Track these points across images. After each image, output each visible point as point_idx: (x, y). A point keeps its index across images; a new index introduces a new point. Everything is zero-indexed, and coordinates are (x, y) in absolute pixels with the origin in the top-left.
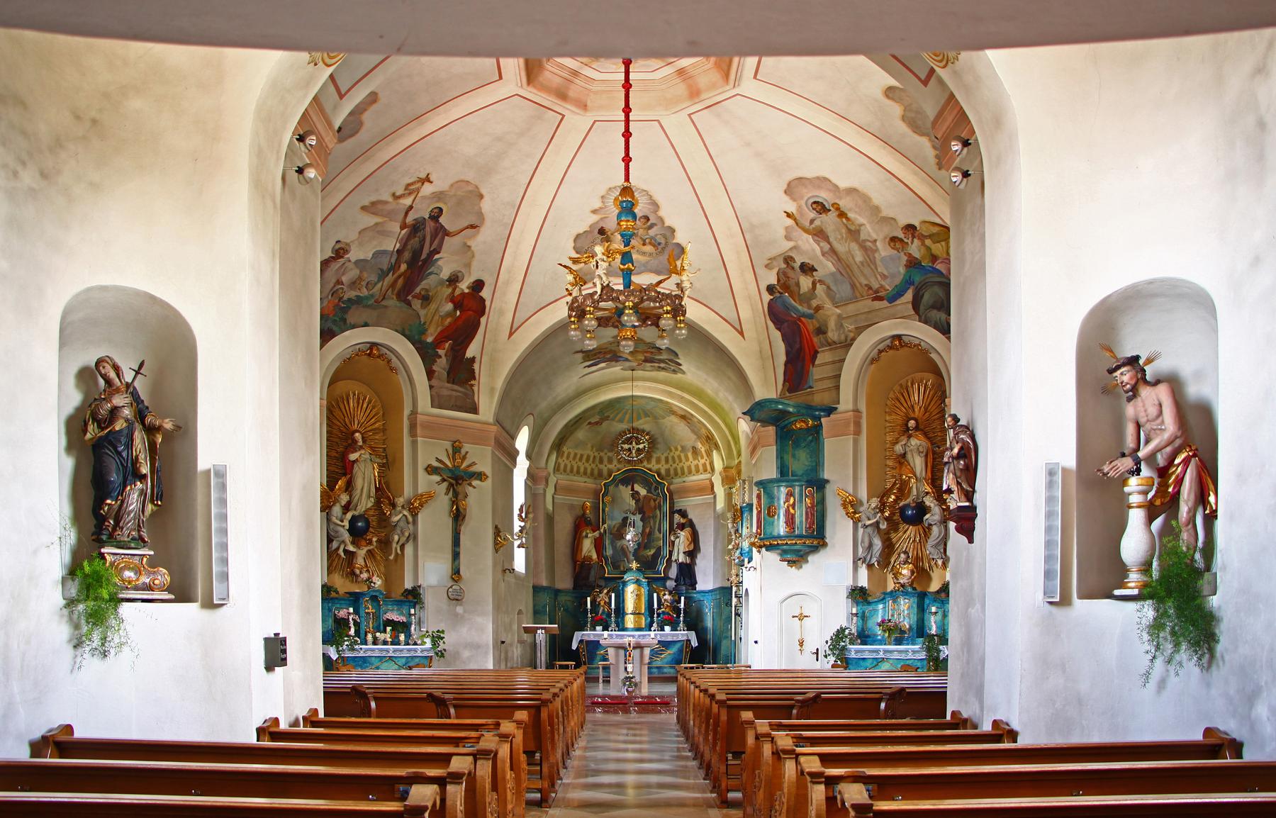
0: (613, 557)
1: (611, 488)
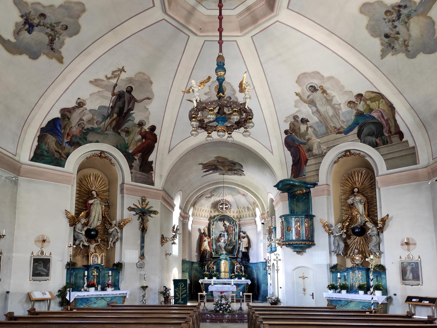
0: (216, 249)
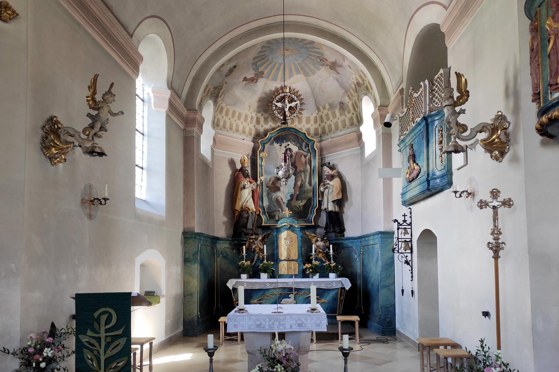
0: (269, 207)
1: (267, 146)
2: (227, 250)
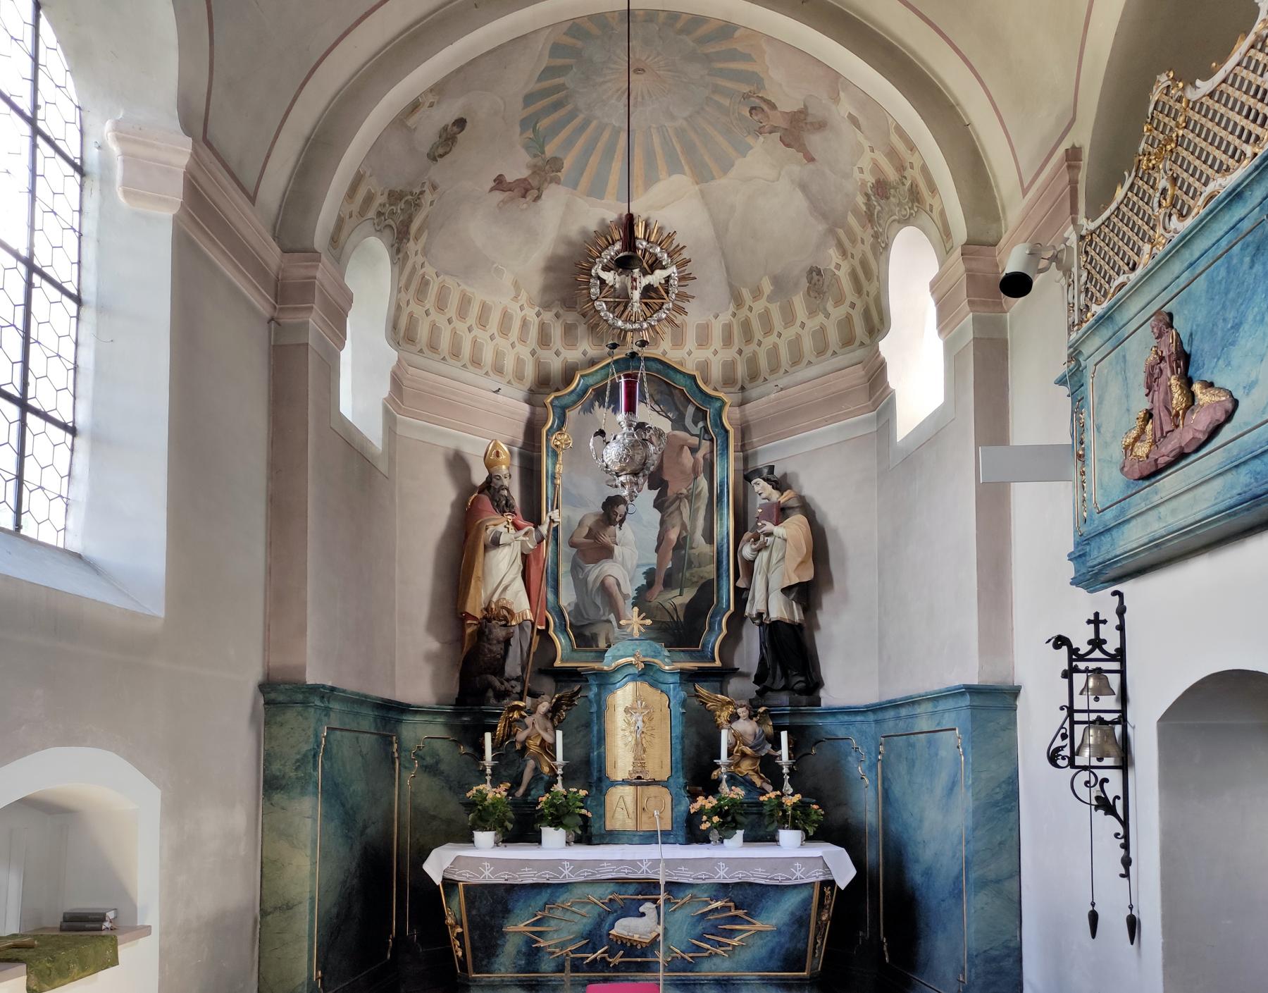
0: (578, 610)
1: (572, 414)
2: (438, 745)
